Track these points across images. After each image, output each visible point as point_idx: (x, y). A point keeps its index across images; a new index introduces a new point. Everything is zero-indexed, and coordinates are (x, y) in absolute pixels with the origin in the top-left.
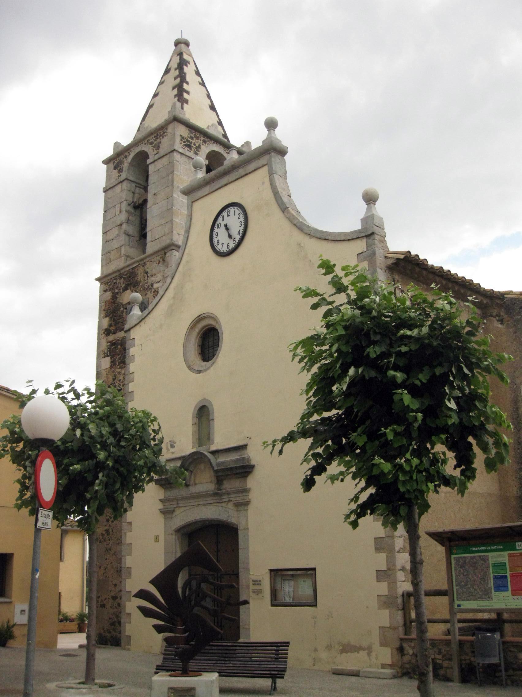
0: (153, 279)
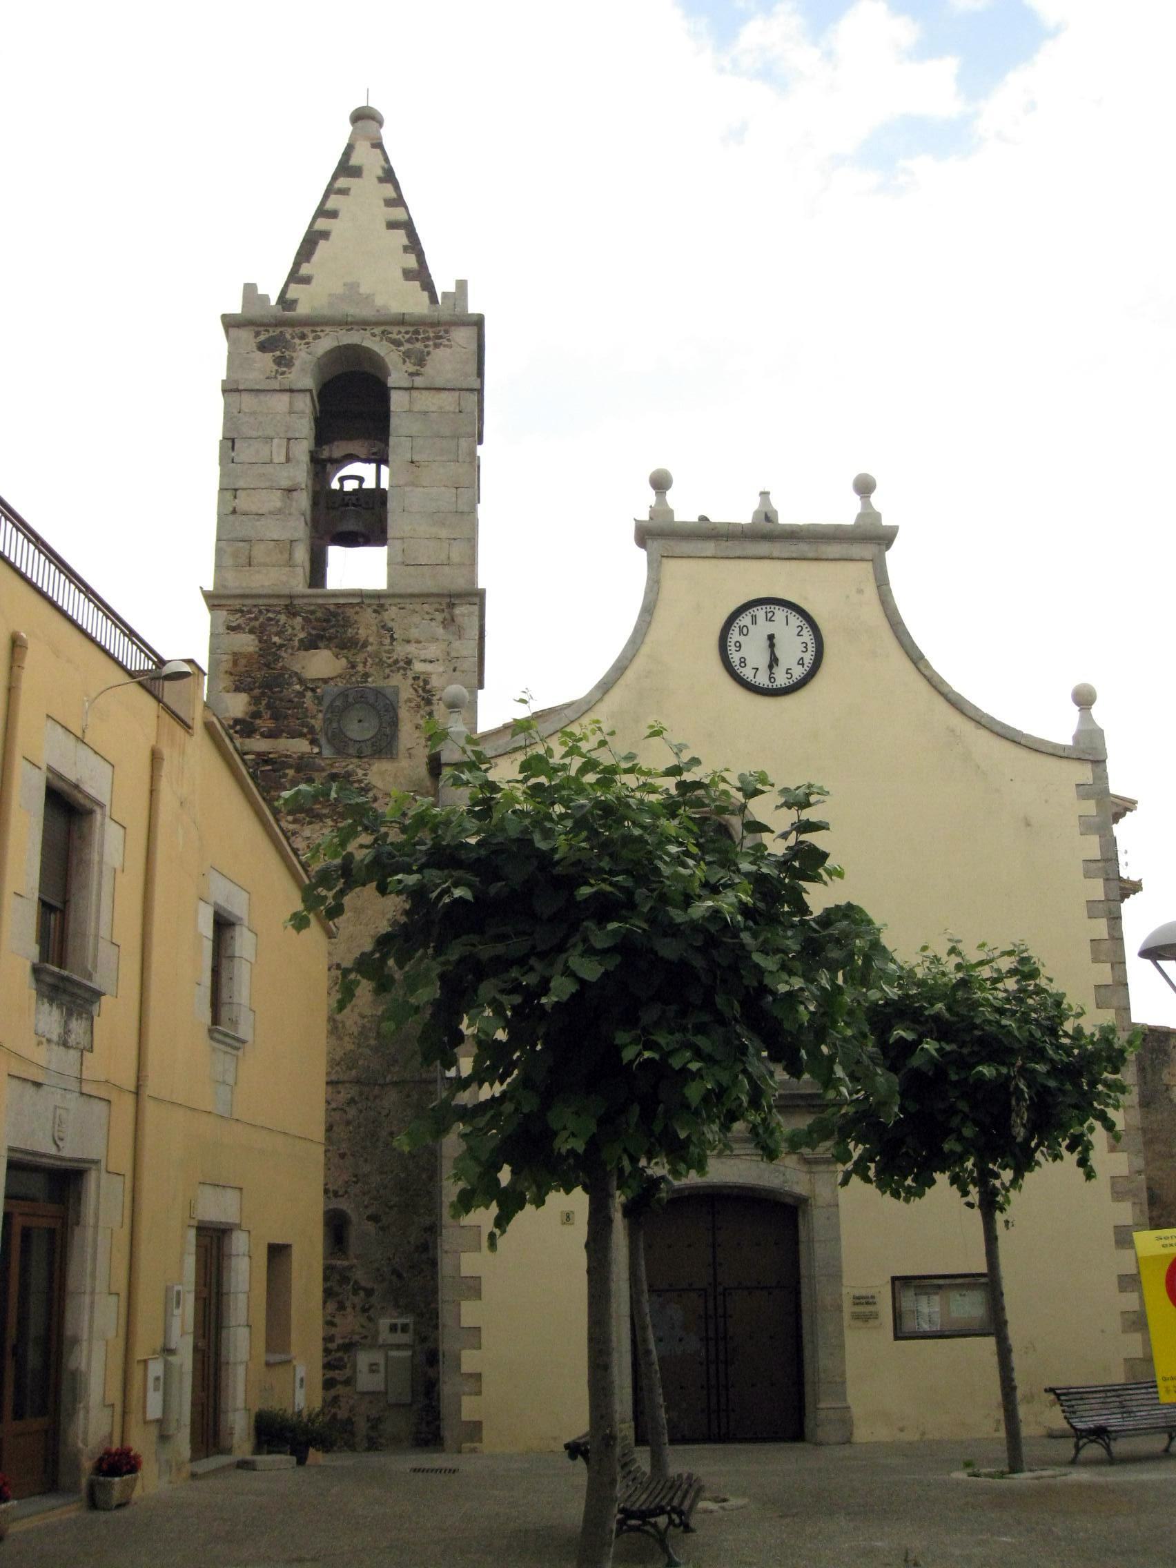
0: (411, 649)
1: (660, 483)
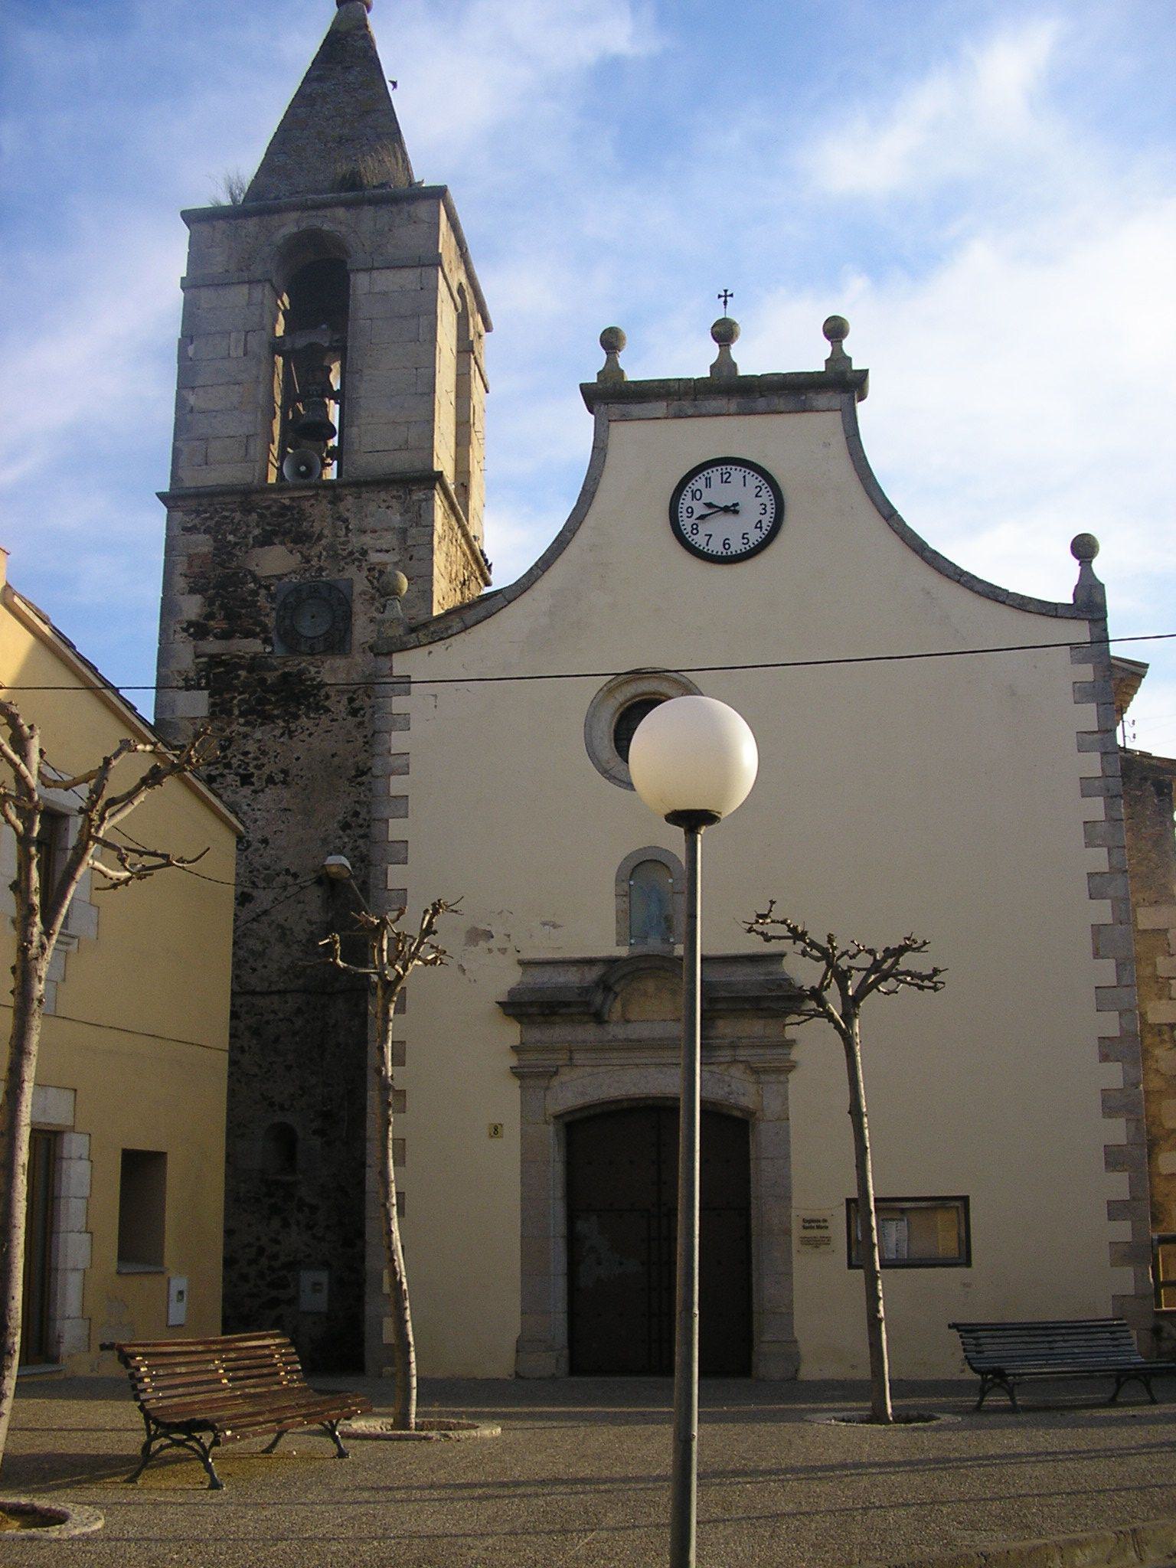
0: (367, 540)
1: (611, 341)
